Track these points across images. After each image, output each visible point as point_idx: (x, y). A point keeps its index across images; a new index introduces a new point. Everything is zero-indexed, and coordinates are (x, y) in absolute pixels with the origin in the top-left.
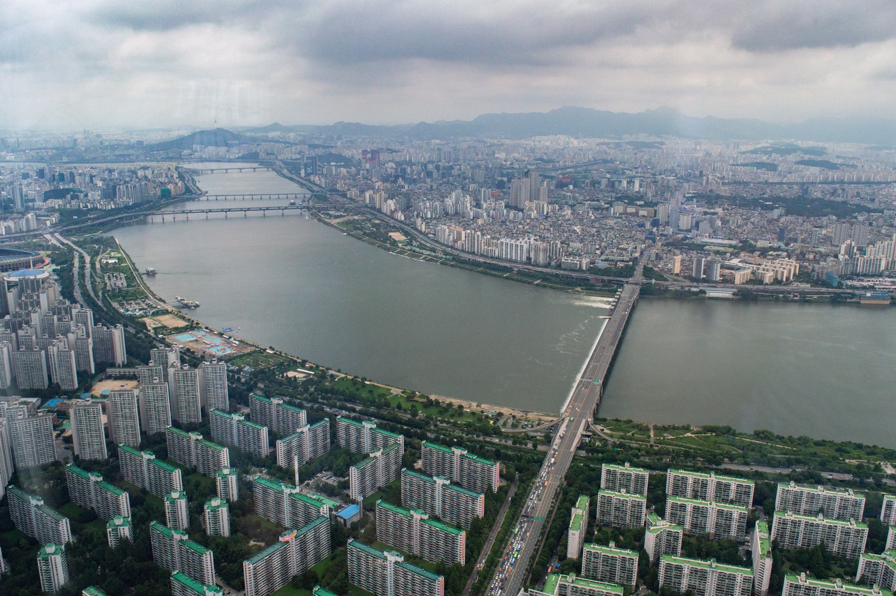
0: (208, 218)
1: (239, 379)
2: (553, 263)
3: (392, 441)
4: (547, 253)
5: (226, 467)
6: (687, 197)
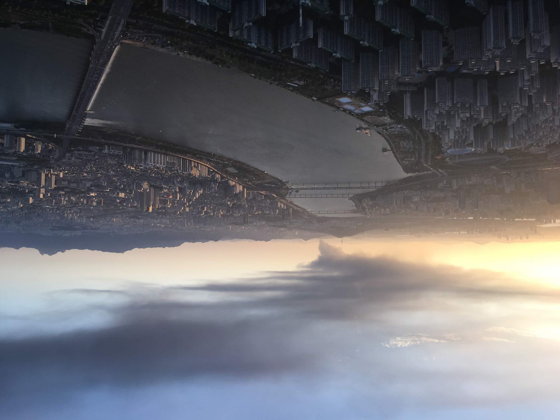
0: (381, 183)
1: (335, 81)
2: (129, 150)
3: (237, 33)
4: (133, 157)
5: (346, 20)
6: (32, 193)
